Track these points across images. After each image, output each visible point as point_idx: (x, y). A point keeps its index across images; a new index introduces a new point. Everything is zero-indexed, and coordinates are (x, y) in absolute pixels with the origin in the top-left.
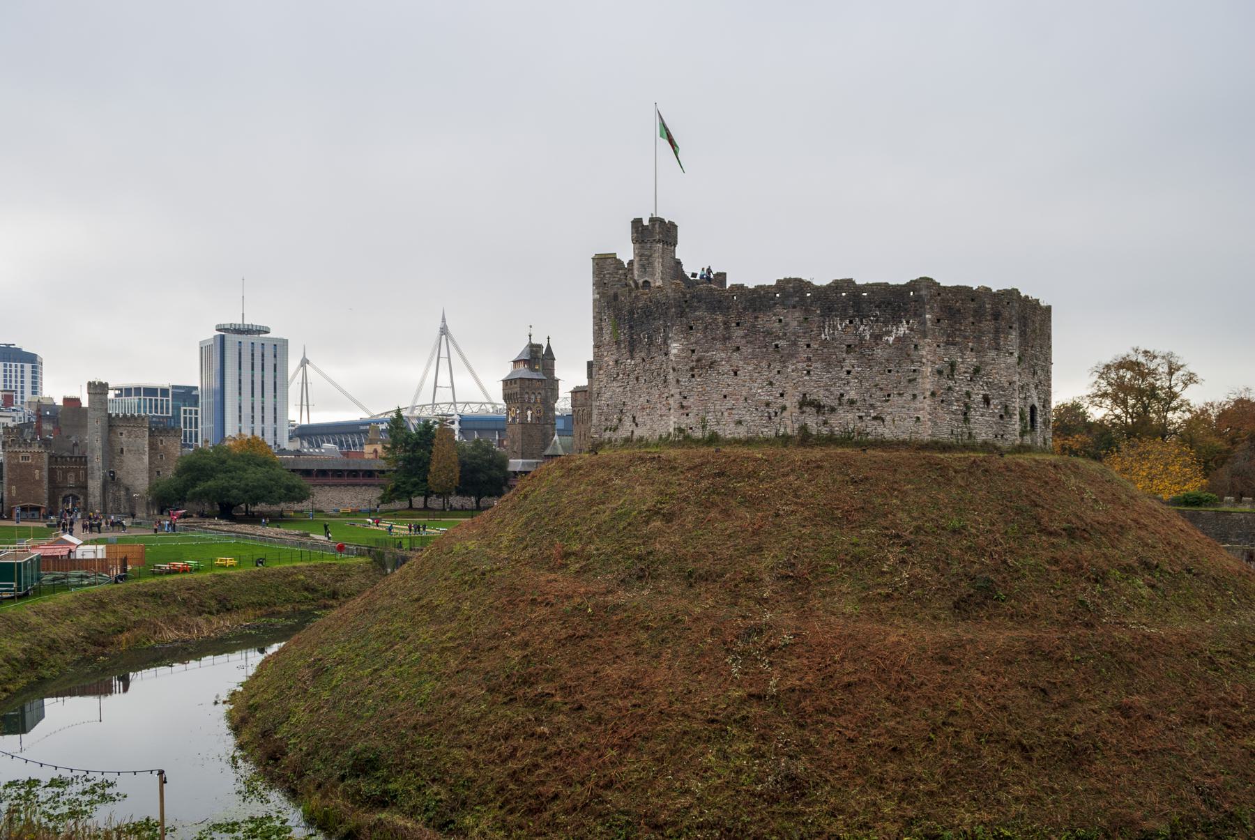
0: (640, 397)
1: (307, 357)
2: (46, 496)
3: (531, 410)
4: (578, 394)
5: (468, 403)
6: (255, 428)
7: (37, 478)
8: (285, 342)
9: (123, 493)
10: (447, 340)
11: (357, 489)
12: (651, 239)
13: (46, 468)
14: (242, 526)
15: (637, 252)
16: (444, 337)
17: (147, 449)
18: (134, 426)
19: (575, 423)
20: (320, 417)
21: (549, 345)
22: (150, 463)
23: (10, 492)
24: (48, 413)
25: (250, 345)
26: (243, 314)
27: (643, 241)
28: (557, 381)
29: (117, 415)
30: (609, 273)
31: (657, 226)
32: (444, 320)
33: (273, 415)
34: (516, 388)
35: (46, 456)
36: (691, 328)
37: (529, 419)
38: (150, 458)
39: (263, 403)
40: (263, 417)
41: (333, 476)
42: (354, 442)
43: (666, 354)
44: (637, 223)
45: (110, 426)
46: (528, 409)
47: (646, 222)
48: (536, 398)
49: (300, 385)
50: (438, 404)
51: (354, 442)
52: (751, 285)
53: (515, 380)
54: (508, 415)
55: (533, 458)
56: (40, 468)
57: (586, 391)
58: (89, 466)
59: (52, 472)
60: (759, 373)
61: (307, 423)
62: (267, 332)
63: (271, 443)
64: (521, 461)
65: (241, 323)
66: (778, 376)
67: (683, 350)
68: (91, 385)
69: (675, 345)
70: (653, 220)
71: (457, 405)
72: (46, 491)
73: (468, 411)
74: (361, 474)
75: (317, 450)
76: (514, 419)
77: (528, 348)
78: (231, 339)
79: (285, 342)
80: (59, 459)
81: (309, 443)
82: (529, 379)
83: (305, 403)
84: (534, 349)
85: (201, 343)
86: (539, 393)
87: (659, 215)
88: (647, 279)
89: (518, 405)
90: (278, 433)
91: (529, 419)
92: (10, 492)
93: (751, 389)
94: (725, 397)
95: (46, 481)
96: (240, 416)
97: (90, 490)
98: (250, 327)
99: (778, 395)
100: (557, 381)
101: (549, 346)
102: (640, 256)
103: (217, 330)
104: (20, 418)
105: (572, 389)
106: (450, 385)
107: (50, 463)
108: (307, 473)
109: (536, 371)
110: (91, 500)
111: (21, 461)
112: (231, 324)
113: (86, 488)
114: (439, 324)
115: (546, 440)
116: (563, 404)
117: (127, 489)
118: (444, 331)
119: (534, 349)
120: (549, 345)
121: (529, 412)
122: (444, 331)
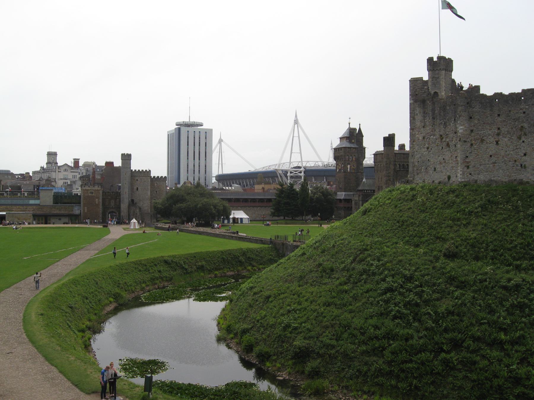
0: (439, 157)
1: (222, 138)
2: (101, 212)
3: (350, 165)
4: (378, 155)
5: (308, 162)
6: (195, 176)
7: (97, 203)
8: (211, 130)
9: (138, 210)
10: (298, 127)
11: (255, 208)
12: (438, 68)
13: (101, 198)
14: (132, 233)
15: (430, 76)
16: (296, 125)
17: (149, 188)
18: (143, 176)
19: (376, 172)
20: (229, 169)
21: (360, 129)
22: (151, 195)
23: (84, 210)
24: (98, 170)
25: (193, 132)
26: (190, 116)
27: (434, 70)
28: (365, 148)
29: (135, 170)
30: (419, 89)
31: (442, 61)
32: (296, 116)
33: (204, 169)
34: (342, 153)
35: (101, 192)
36: (471, 118)
37: (349, 170)
38: (151, 192)
39: (199, 163)
40: (199, 171)
41: (266, 202)
42: (246, 183)
43: (455, 133)
44: (430, 60)
45: (132, 176)
46: (348, 164)
47: (435, 59)
48: (353, 158)
49: (218, 153)
50: (292, 162)
51: (246, 183)
52: (506, 92)
53: (341, 148)
54: (336, 168)
55: (351, 192)
56: (98, 198)
57: (383, 154)
58: (121, 197)
59: (103, 200)
60: (512, 142)
61: (221, 173)
62: (202, 125)
63: (203, 184)
64: (344, 193)
65: (188, 121)
66: (523, 144)
67: (466, 130)
68: (123, 155)
69: (462, 127)
70: (439, 58)
71: (303, 163)
72: (101, 210)
73: (308, 165)
74: (241, 200)
75: (230, 188)
76: (340, 170)
77: (348, 131)
78: (184, 130)
79: (211, 130)
80: (107, 193)
81: (222, 184)
82: (349, 148)
83: (220, 163)
84: (352, 131)
85: (168, 132)
86: (354, 155)
87: (442, 55)
88: (436, 91)
89: (342, 162)
90: (207, 179)
91: (349, 170)
92: (84, 210)
93: (506, 151)
94: (491, 156)
95: (101, 204)
96: (188, 170)
97: (122, 209)
98: (193, 123)
99: (522, 155)
100: (365, 148)
101: (360, 129)
102: (432, 78)
103: (177, 125)
104: (82, 173)
105: (374, 153)
106: (299, 151)
107: (103, 196)
108: (229, 200)
109: (353, 143)
110: (122, 214)
111: (89, 194)
112: (184, 122)
113: (120, 208)
114: (293, 118)
115: (358, 181)
116: (369, 160)
117: (140, 208)
118: (296, 122)
119: (352, 131)
120: (360, 129)
121: (349, 166)
122: (296, 122)
